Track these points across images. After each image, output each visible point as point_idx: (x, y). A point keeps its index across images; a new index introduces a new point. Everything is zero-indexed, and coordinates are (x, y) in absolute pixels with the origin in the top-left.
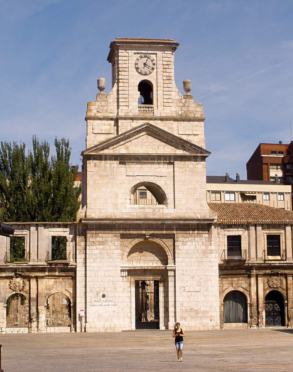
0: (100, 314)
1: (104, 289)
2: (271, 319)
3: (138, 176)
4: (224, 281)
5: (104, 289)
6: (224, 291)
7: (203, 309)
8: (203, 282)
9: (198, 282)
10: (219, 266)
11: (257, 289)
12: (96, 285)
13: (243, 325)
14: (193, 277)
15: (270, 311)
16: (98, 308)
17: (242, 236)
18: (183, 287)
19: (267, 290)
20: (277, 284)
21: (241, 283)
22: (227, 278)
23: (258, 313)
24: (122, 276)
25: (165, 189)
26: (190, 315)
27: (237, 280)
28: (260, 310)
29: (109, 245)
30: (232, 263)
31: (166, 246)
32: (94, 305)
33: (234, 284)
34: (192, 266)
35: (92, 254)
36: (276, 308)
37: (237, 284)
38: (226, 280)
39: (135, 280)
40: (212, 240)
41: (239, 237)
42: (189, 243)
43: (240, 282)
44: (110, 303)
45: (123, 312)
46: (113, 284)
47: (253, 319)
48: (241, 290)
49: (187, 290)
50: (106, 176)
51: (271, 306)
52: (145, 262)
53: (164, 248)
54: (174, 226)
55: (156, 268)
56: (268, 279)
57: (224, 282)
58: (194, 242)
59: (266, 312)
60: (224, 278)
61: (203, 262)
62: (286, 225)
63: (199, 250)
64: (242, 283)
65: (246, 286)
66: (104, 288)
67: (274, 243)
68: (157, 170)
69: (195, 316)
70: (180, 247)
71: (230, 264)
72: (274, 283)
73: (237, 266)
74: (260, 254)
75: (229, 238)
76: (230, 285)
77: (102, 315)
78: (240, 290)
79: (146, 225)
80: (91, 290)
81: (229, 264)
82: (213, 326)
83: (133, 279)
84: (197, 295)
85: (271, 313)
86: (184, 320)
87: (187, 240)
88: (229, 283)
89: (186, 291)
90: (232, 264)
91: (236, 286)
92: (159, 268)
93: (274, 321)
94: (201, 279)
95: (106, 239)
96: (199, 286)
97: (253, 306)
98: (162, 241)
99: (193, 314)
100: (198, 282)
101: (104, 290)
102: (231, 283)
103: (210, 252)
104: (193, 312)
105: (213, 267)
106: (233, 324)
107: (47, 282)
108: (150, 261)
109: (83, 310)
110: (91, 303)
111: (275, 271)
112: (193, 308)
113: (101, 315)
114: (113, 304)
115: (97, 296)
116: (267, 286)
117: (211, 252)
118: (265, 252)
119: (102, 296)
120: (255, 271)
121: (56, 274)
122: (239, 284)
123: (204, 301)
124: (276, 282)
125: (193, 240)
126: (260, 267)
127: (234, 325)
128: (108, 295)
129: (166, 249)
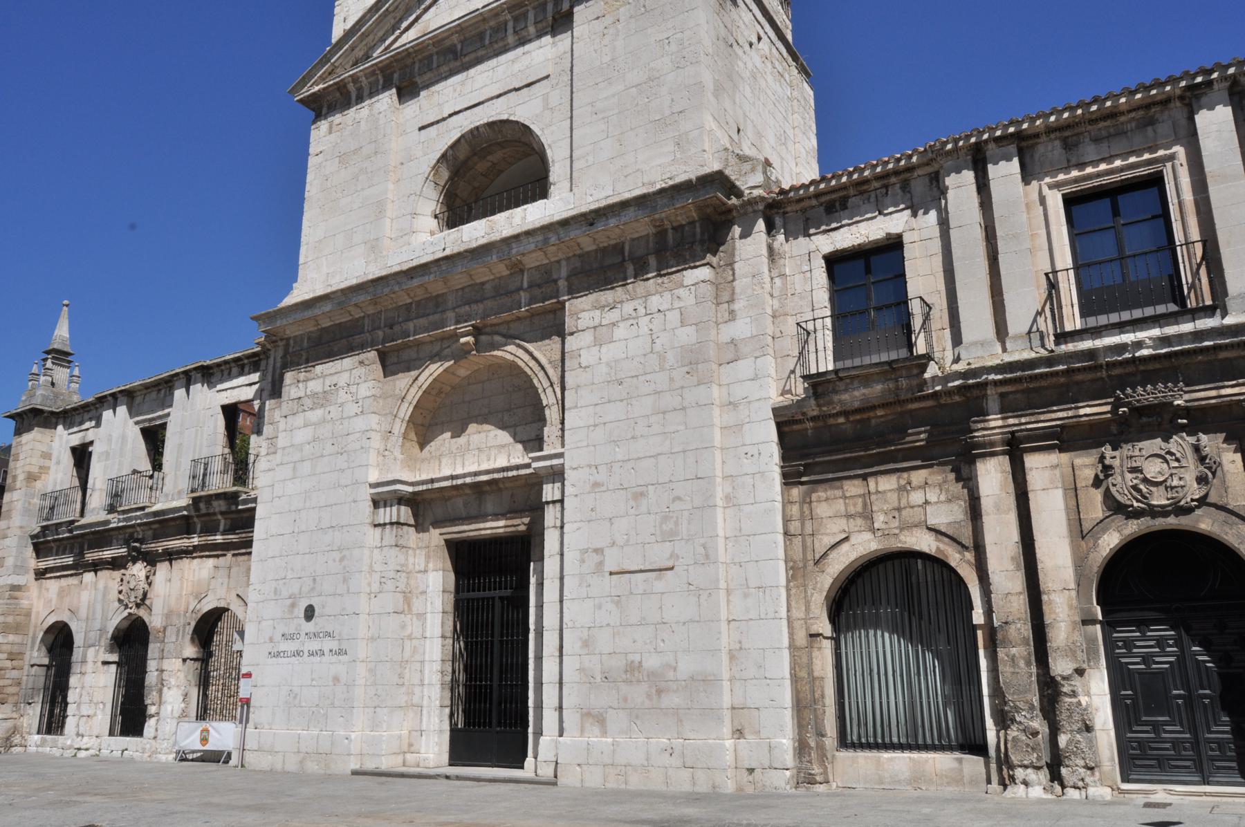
2: (1173, 732)
3: (455, 117)
4: (819, 501)
6: (825, 555)
7: (687, 666)
8: (686, 514)
9: (665, 519)
10: (779, 425)
11: (1039, 530)
13: (955, 765)
14: (639, 496)
15: (1161, 673)
17: (906, 239)
18: (596, 551)
19: (1104, 531)
20: (1175, 482)
21: (921, 501)
22: (838, 483)
23: (1051, 692)
24: (379, 525)
25: (542, 130)
26: (625, 700)
27: (896, 486)
28: (1060, 666)
29: (340, 401)
30: (846, 390)
31: (536, 368)
32: (278, 655)
33: (881, 510)
34: (633, 438)
35: (292, 445)
36: (1130, 654)
37: (899, 509)
38: (830, 493)
39: (446, 541)
40: (738, 290)
41: (894, 245)
42: (621, 332)
43: (917, 497)
44: (328, 644)
45: (162, 671)
46: (342, 560)
47: (1013, 732)
48: (925, 543)
49: (611, 565)
50: (356, 151)
51: (1161, 642)
52: (483, 457)
53: (533, 376)
54: (559, 269)
55: (505, 474)
56: (1102, 458)
57: (822, 510)
58: (644, 321)
59: (1119, 678)
60: (821, 487)
61: (684, 409)
62: (1194, 97)
63: (670, 356)
64: (927, 502)
65: (951, 519)
67: (1126, 237)
68: (517, 67)
69: (647, 703)
70: (586, 358)
71: (836, 398)
72: (1146, 480)
73: (883, 406)
74: (1024, 304)
75: (834, 261)
76: (859, 521)
78: (917, 548)
79: (460, 293)
81: (830, 403)
82: (751, 771)
83: (435, 537)
84: (659, 586)
85: (1167, 691)
86: (596, 730)
87: (614, 315)
88: (852, 510)
89: (608, 568)
90: (845, 397)
91: (896, 523)
92: (514, 473)
93: (1196, 744)
94: (679, 498)
95: (335, 379)
96: (669, 537)
97: (1007, 643)
98: (531, 354)
99: (638, 694)
100: (665, 519)
101: (313, 589)
102: (859, 508)
103: (730, 356)
104: (639, 681)
105: (746, 427)
106: (891, 759)
108: (485, 452)
111: (1145, 395)
112: (637, 664)
114: (334, 645)
116: (1095, 508)
117: (733, 352)
118: (1052, 304)
120: (995, 421)
122: (910, 509)
123: (692, 621)
124: (1163, 468)
125: (642, 311)
126: (1027, 387)
127: (899, 762)
129: (540, 382)
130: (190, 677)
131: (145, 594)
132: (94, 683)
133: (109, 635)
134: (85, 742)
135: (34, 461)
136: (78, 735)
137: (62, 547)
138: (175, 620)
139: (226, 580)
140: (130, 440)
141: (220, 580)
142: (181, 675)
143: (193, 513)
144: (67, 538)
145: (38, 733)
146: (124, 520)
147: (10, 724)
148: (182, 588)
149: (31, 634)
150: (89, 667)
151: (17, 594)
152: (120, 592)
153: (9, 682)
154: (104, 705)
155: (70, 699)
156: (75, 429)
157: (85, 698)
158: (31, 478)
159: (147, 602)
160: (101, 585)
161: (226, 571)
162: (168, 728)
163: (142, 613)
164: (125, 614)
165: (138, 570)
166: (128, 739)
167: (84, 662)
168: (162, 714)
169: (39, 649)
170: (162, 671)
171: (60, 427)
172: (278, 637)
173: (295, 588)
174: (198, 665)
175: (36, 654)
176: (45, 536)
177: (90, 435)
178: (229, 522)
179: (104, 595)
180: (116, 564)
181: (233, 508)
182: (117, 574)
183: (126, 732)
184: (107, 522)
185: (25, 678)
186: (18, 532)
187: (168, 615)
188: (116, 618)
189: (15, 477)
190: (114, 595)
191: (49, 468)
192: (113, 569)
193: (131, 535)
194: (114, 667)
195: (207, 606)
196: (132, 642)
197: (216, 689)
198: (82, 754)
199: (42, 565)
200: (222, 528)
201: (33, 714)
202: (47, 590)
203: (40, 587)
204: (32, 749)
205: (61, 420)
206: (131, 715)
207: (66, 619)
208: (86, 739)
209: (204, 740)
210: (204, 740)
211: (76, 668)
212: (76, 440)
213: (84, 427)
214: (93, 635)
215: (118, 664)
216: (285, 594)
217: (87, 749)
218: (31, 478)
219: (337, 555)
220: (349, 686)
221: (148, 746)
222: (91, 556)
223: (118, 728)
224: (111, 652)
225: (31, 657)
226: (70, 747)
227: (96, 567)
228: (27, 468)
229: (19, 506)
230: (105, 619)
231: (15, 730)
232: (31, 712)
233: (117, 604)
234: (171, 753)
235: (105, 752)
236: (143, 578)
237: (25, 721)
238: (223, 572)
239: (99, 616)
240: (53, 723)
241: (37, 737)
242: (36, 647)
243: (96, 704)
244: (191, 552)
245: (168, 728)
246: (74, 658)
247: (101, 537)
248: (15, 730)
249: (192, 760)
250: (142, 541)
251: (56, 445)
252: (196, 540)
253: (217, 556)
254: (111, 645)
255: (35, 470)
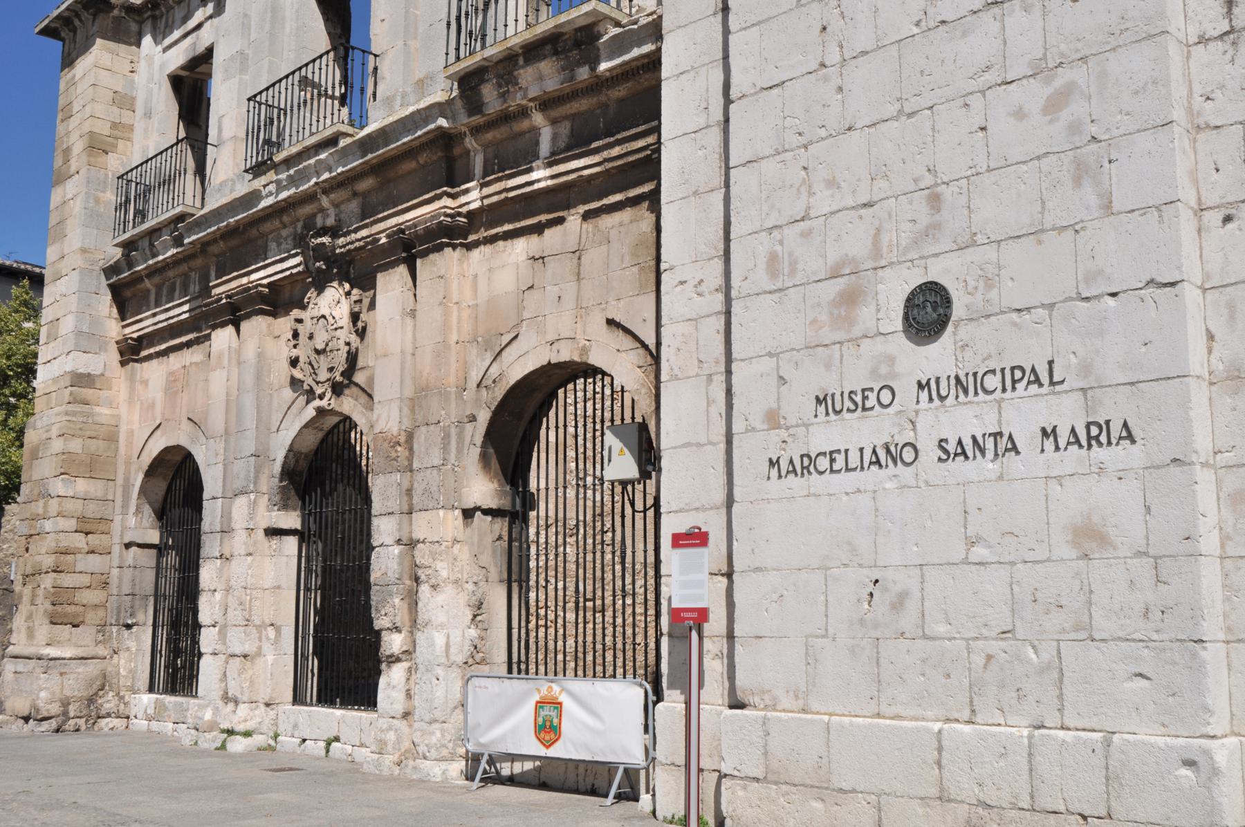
0: (887, 575)
1: (924, 218)
5: (924, 218)
12: (832, 183)
16: (865, 500)
32: (807, 465)
44: (1024, 414)
45: (412, 544)
46: (1053, 106)
66: (935, 201)
77: (912, 606)
80: (773, 259)
101: (932, 231)
107: (198, 204)
109: (679, 540)
110: (776, 436)
113: (899, 603)
114: (1067, 413)
115: (849, 321)
119: (898, 324)
121: (535, 175)
128: (989, 283)
130: (486, 559)
131: (352, 359)
132: (254, 578)
133: (277, 467)
134: (241, 717)
135: (100, 110)
136: (226, 698)
137: (166, 281)
138: (435, 409)
139: (571, 287)
140: (289, 13)
141: (552, 291)
142: (463, 553)
143: (464, 120)
144: (175, 262)
145: (151, 689)
146: (292, 181)
147: (92, 668)
148: (446, 327)
149: (120, 481)
150: (239, 542)
151: (87, 393)
152: (294, 362)
153: (85, 580)
154: (278, 630)
155: (204, 617)
156: (177, 34)
157: (235, 615)
158: (98, 147)
159: (359, 378)
160: (250, 352)
161: (569, 263)
162: (439, 693)
163: (348, 405)
164: (310, 412)
165: (333, 302)
166: (339, 713)
167: (226, 531)
168: (422, 653)
169: (138, 510)
170: (412, 544)
171: (147, 40)
172: (799, 405)
173: (853, 240)
174: (501, 526)
175: (132, 521)
176: (130, 265)
177: (205, 38)
178: (565, 129)
179: (259, 377)
180: (279, 300)
181: (583, 73)
182: (284, 325)
183: (327, 697)
184: (254, 196)
185: (115, 572)
186: (78, 261)
187: (416, 402)
188: (288, 427)
189: (67, 151)
190: (282, 371)
191: (131, 128)
192: (274, 314)
193: (309, 223)
194: (292, 543)
195: (520, 364)
196: (326, 478)
197: (593, 591)
198: (238, 745)
199: (133, 331)
200: (545, 148)
201: (136, 650)
202: (145, 383)
203: (132, 379)
204: (140, 724)
205: (148, 26)
206: (343, 660)
207: (184, 441)
208: (243, 710)
209: (548, 730)
210: (548, 730)
211: (210, 546)
212: (177, 58)
213: (192, 24)
214: (242, 469)
215: (301, 535)
216: (812, 263)
217: (247, 734)
218: (98, 147)
219: (1033, 94)
220: (1164, 561)
221: (391, 736)
222: (223, 289)
223: (312, 685)
224: (285, 506)
225: (124, 528)
226: (212, 726)
227: (233, 314)
228: (86, 127)
229: (77, 207)
230: (265, 430)
231: (104, 683)
232: (133, 645)
233: (288, 394)
234: (452, 758)
235: (288, 742)
236: (345, 321)
237: (122, 664)
238: (559, 268)
239: (250, 423)
240: (177, 670)
241: (147, 699)
242: (133, 509)
243: (261, 627)
244: (463, 232)
245: (439, 693)
246: (205, 526)
247: (241, 238)
248: (104, 683)
249: (512, 781)
250: (335, 232)
251: (140, 79)
252: (473, 197)
253: (538, 229)
254: (283, 490)
255: (103, 129)
